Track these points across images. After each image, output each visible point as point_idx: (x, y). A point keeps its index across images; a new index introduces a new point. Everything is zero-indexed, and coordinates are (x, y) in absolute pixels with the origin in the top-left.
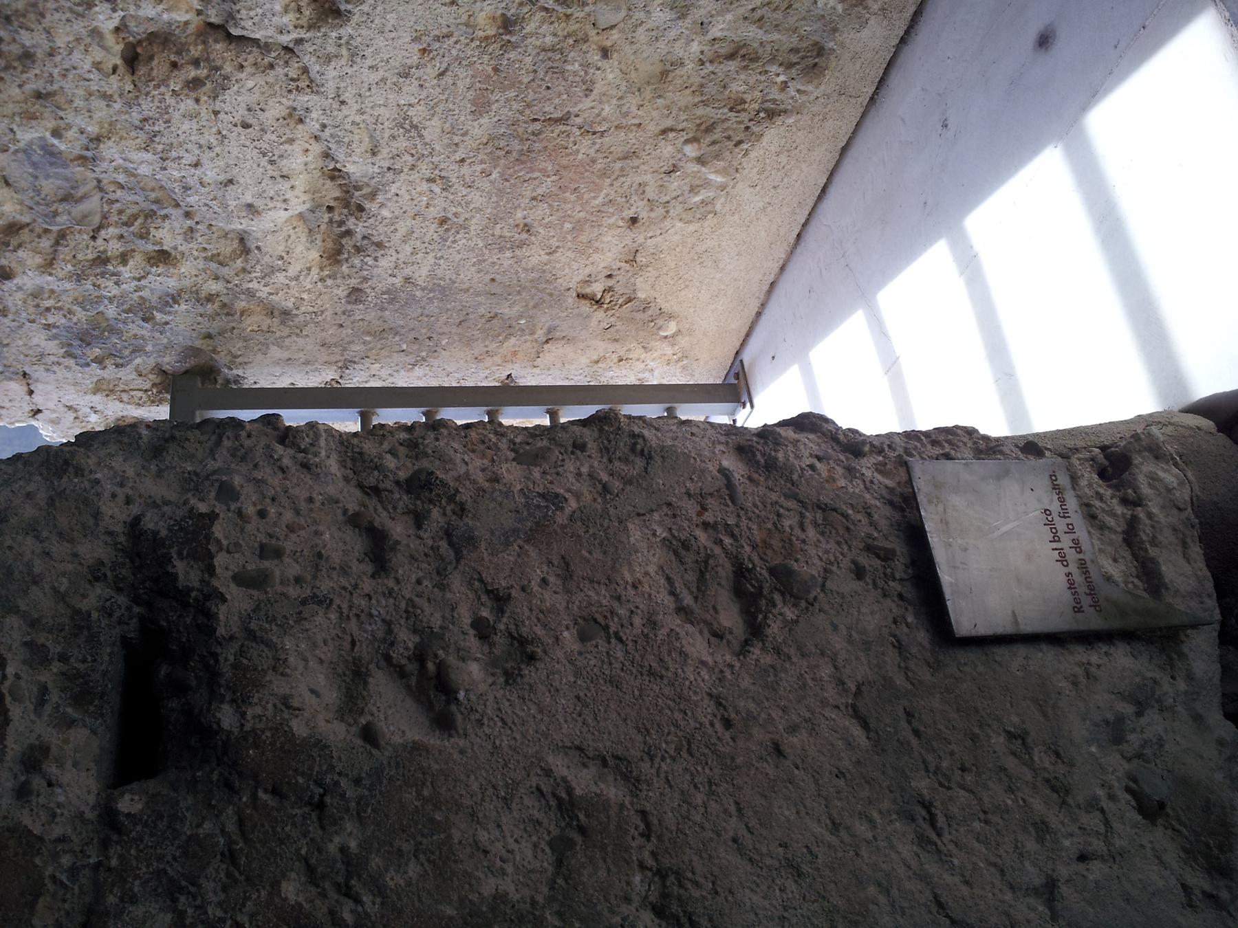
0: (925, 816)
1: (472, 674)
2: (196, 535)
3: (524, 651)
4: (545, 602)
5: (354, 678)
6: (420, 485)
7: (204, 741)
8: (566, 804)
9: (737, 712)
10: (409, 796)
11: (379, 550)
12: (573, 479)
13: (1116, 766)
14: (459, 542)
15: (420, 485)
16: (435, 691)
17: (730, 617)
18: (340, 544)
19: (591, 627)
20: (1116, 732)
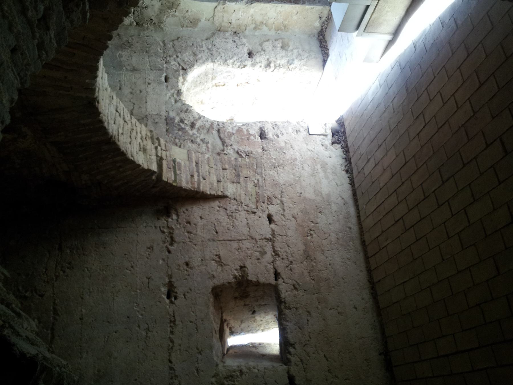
0: (307, 144)
1: (280, 135)
2: (264, 127)
3: (283, 134)
4: (284, 132)
5: (273, 135)
6: (276, 125)
7: (265, 138)
8: (286, 142)
9: (13, 70)
10: (295, 17)
11: (274, 128)
12: (286, 124)
13: (321, 143)
14: (278, 128)
15: (276, 125)
16: (278, 136)
17: (296, 133)
18: (272, 128)
19: (287, 133)
20: (321, 141)
